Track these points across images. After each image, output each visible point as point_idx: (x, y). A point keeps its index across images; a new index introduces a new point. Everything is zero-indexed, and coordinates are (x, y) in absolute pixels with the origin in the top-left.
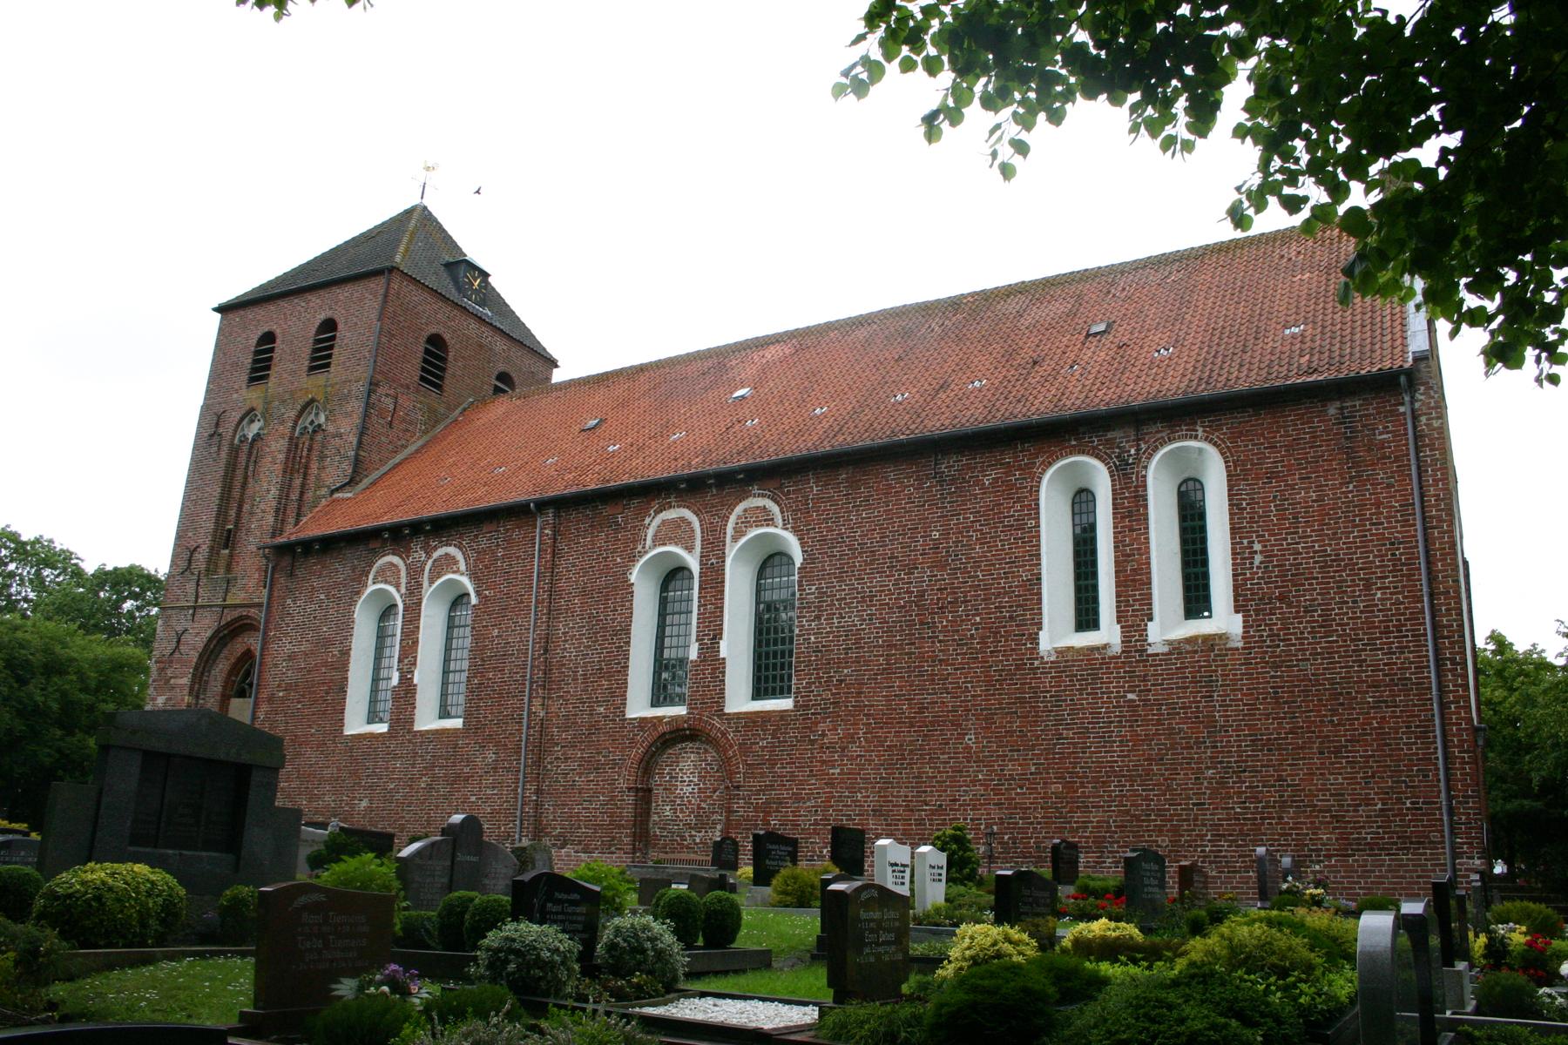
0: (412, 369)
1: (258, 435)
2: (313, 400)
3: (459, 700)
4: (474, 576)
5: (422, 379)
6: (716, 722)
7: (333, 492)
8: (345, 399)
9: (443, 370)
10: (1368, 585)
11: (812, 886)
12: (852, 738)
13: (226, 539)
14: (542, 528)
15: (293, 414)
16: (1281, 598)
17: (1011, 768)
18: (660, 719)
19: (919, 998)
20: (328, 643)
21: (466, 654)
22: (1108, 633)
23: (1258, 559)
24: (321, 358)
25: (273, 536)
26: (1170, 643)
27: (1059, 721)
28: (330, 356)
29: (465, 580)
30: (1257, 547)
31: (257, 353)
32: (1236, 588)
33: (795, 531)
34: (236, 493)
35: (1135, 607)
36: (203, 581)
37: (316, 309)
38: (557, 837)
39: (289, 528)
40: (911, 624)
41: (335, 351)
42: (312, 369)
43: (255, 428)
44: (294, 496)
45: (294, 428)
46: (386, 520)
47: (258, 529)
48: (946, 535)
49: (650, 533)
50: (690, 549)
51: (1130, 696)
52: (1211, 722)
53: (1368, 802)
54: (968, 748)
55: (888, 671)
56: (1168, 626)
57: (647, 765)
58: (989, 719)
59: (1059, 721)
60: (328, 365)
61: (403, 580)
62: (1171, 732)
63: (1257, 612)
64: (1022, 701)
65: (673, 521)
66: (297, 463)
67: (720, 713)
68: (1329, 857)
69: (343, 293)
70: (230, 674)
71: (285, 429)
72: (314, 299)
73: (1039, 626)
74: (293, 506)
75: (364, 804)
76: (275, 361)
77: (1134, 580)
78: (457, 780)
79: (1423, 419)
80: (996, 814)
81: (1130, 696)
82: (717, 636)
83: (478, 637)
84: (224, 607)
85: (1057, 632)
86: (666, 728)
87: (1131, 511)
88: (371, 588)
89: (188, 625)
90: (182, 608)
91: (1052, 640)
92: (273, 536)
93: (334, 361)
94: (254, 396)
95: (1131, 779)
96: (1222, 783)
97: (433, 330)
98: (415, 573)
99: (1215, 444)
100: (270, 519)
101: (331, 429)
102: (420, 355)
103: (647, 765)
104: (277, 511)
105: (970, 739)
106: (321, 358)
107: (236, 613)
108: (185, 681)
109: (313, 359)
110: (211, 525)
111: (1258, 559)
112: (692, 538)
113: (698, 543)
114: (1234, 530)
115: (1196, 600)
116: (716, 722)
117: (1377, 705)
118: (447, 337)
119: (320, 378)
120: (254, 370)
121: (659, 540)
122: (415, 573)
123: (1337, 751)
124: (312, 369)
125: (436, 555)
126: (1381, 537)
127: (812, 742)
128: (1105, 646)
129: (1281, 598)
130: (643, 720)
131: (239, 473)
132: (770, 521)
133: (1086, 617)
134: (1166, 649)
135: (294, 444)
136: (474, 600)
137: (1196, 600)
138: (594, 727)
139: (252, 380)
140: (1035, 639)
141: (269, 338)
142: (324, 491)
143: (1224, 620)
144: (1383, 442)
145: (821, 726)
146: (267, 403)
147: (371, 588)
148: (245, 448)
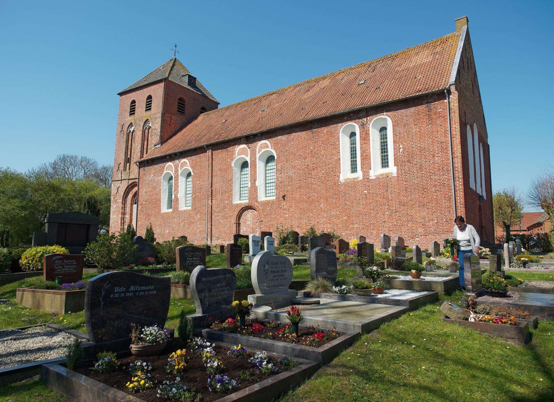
0: (175, 108)
1: (134, 130)
2: (147, 120)
3: (190, 202)
4: (192, 167)
5: (178, 111)
6: (256, 204)
7: (155, 146)
8: (155, 119)
9: (184, 108)
10: (434, 157)
11: (344, 246)
12: (291, 206)
13: (128, 160)
14: (209, 153)
15: (143, 124)
16: (408, 161)
17: (333, 213)
18: (241, 204)
19: (373, 278)
20: (155, 188)
21: (190, 189)
22: (359, 174)
23: (401, 150)
24: (148, 107)
25: (141, 158)
26: (376, 176)
27: (346, 199)
28: (151, 106)
29: (190, 168)
30: (401, 146)
31: (131, 107)
32: (395, 159)
33: (275, 149)
34: (129, 147)
35: (366, 165)
36: (123, 173)
37: (146, 92)
38: (217, 237)
39: (144, 157)
40: (305, 174)
41: (152, 105)
42: (146, 110)
43: (133, 128)
44: (145, 147)
45: (143, 128)
46: (168, 153)
47: (136, 157)
48: (314, 148)
49: (237, 152)
50: (247, 156)
51: (365, 192)
52: (388, 198)
53: (433, 220)
54: (321, 208)
55: (300, 187)
56: (376, 170)
57: (239, 217)
58: (327, 200)
59: (346, 199)
60: (150, 109)
61: (174, 169)
62: (376, 201)
63: (401, 165)
64: (336, 194)
65: (242, 148)
66: (145, 138)
67: (257, 201)
68: (421, 236)
69: (152, 87)
70: (133, 198)
71: (141, 128)
72: (145, 90)
73: (340, 173)
74: (145, 150)
75: (167, 231)
76: (136, 108)
77: (366, 158)
78: (191, 223)
79: (452, 104)
80: (329, 226)
81: (365, 192)
82: (255, 180)
83: (194, 184)
84: (129, 179)
85: (345, 174)
86: (243, 206)
87: (365, 138)
88: (165, 172)
89: (120, 185)
90: (118, 181)
91: (374, 173)
92: (141, 158)
93: (152, 107)
94: (130, 119)
95: (365, 215)
96: (391, 215)
97: (180, 96)
98: (176, 167)
99: (389, 116)
100: (139, 154)
101: (153, 127)
102: (177, 104)
103: (239, 217)
104: (141, 152)
105: (322, 205)
106: (148, 107)
107: (132, 181)
108: (121, 200)
109: (146, 108)
110: (124, 157)
111: (401, 150)
112: (247, 153)
113: (249, 154)
114: (394, 142)
115: (385, 163)
116: (256, 204)
117: (436, 191)
118: (184, 98)
119: (149, 113)
120: (130, 112)
121: (239, 154)
122: (176, 167)
123: (424, 206)
124: (146, 110)
125: (181, 162)
126: (438, 142)
127: (281, 208)
128: (358, 178)
129: (408, 161)
130: (237, 204)
131: (130, 142)
132: (267, 147)
133: (354, 169)
134: (375, 178)
135: (144, 132)
136: (192, 174)
137: (385, 163)
138: (225, 207)
139: (130, 114)
140: (339, 176)
141: (134, 102)
142: (153, 145)
143: (392, 169)
144: (440, 112)
145: (283, 204)
146: (135, 120)
147: (165, 172)
148: (131, 134)
